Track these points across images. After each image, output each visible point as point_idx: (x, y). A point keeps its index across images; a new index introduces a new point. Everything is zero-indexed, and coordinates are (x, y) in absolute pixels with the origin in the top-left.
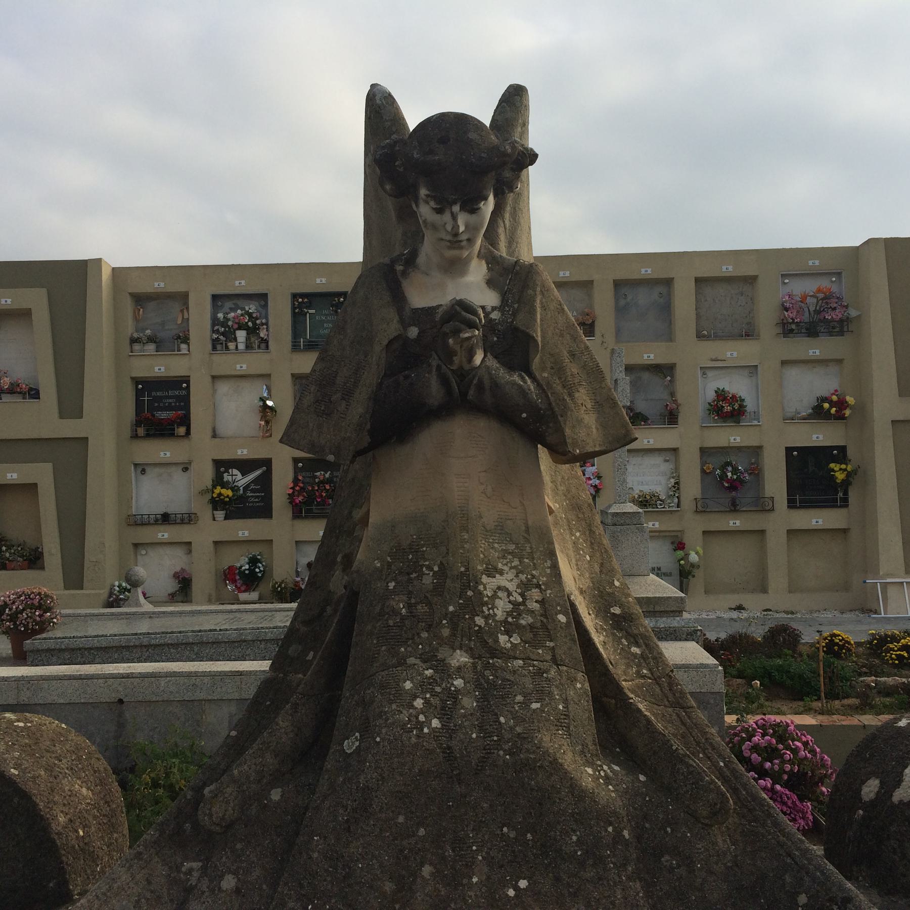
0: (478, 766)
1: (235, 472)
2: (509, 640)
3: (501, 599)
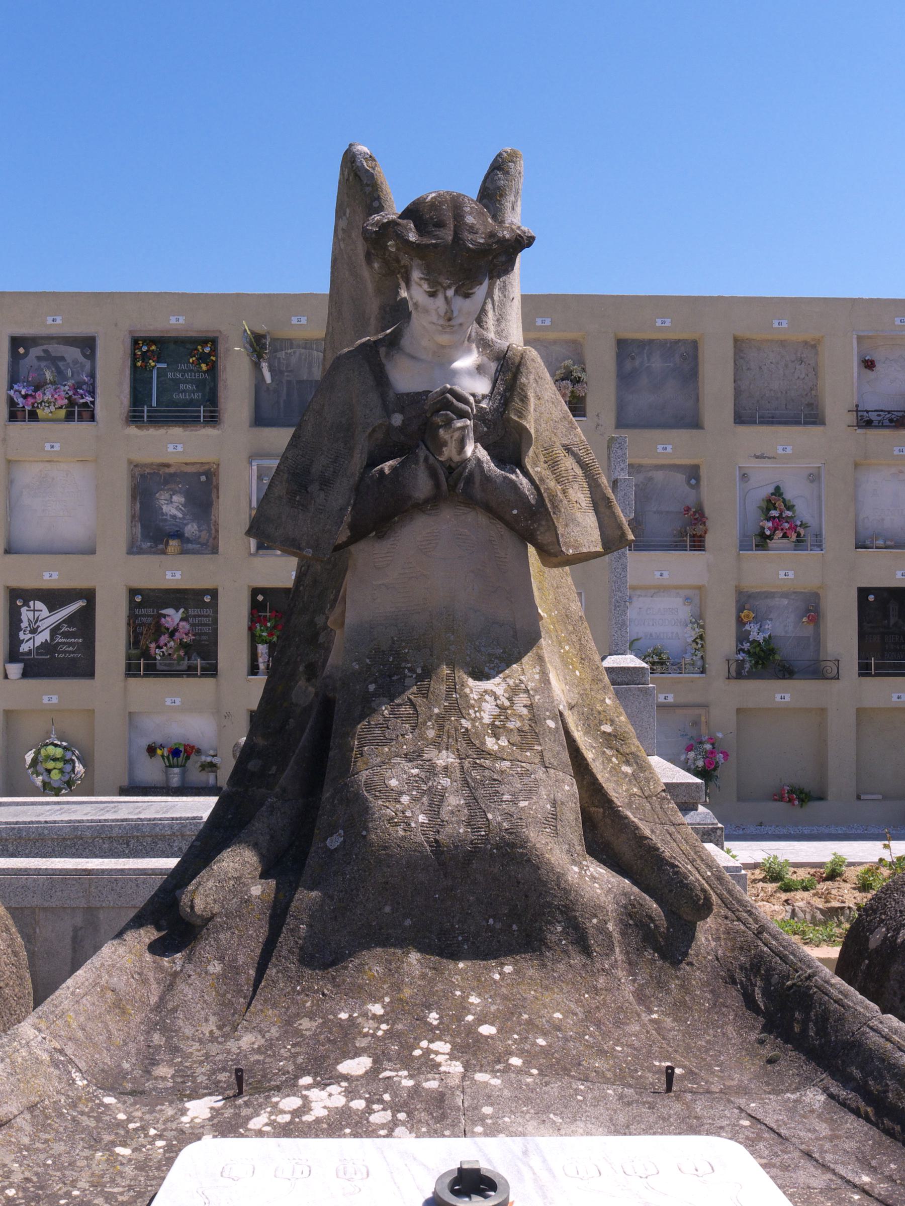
0: (465, 860)
1: (39, 605)
2: (497, 742)
3: (487, 702)
